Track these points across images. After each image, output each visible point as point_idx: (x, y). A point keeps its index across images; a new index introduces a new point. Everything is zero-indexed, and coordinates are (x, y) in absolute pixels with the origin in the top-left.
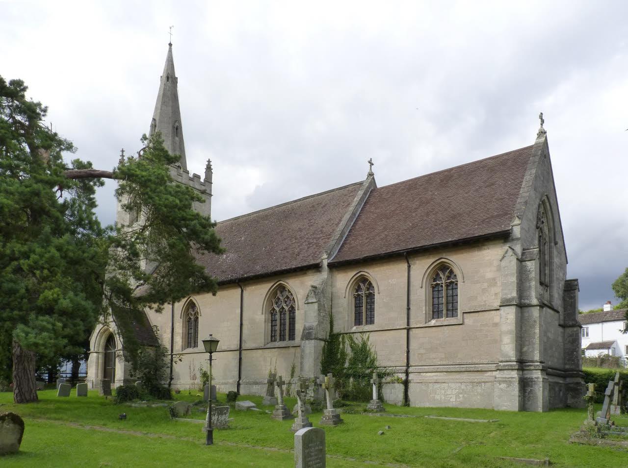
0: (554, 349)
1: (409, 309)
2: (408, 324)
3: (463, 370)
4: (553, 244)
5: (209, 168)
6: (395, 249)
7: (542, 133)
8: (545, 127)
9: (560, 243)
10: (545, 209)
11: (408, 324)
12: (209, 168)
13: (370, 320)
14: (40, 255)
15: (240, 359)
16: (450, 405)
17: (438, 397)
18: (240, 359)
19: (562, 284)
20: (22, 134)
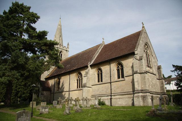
0: (156, 86)
1: (111, 77)
2: (111, 81)
3: (126, 94)
4: (151, 56)
5: (68, 44)
6: (106, 60)
7: (143, 27)
8: (144, 25)
9: (154, 55)
10: (147, 46)
11: (111, 81)
12: (68, 44)
13: (102, 81)
14: (12, 17)
15: (69, 94)
16: (123, 106)
17: (120, 103)
18: (69, 94)
19: (156, 67)
20: (3, 105)
